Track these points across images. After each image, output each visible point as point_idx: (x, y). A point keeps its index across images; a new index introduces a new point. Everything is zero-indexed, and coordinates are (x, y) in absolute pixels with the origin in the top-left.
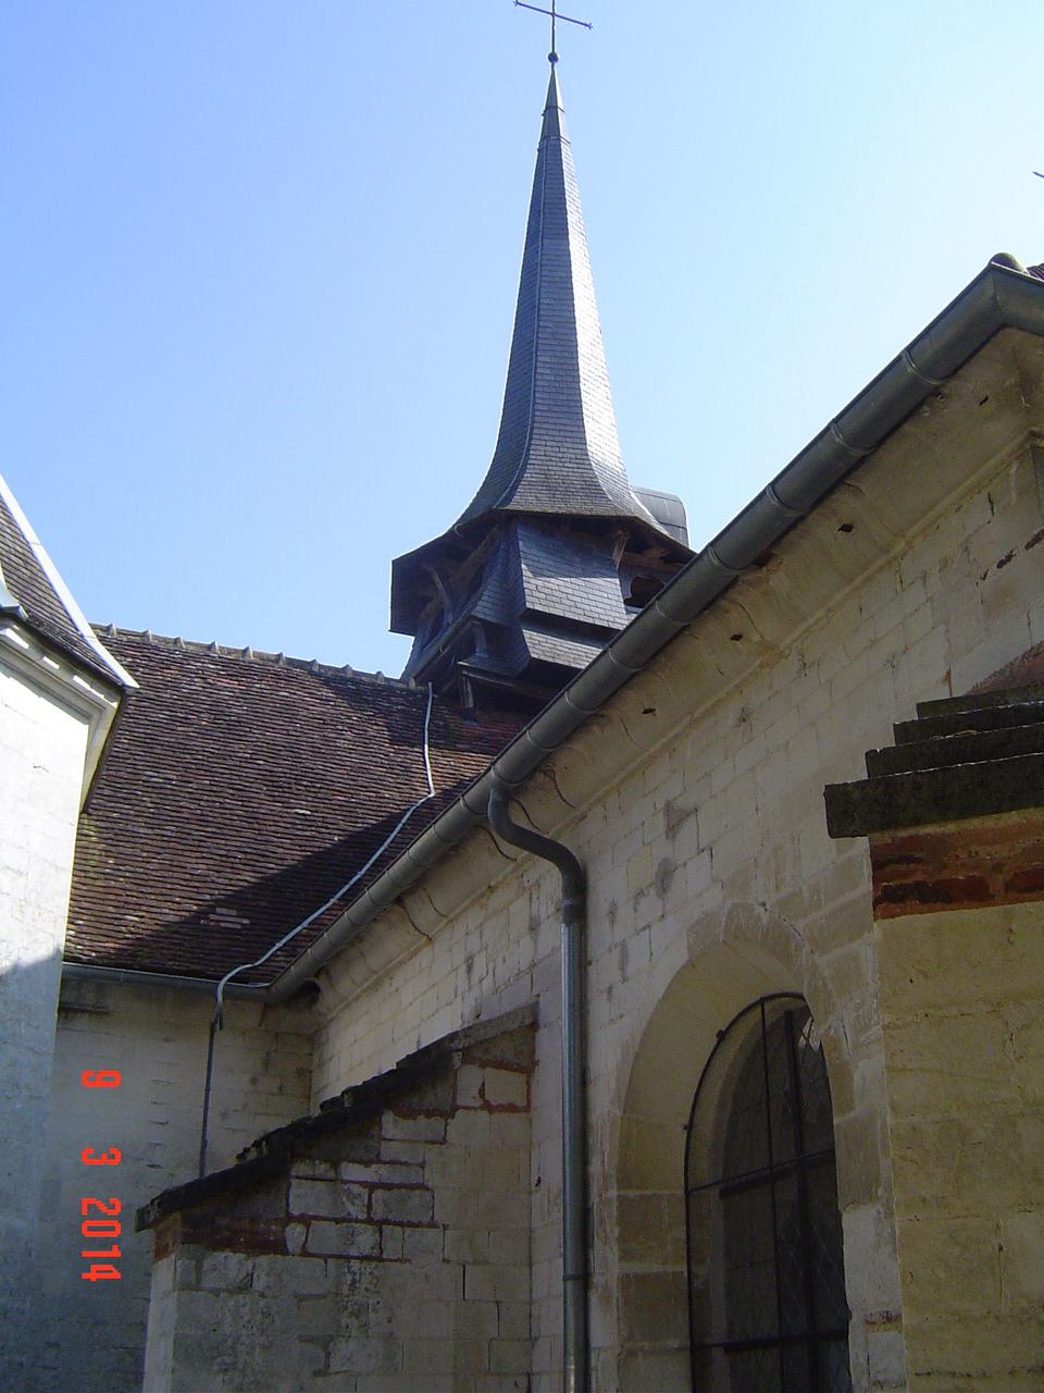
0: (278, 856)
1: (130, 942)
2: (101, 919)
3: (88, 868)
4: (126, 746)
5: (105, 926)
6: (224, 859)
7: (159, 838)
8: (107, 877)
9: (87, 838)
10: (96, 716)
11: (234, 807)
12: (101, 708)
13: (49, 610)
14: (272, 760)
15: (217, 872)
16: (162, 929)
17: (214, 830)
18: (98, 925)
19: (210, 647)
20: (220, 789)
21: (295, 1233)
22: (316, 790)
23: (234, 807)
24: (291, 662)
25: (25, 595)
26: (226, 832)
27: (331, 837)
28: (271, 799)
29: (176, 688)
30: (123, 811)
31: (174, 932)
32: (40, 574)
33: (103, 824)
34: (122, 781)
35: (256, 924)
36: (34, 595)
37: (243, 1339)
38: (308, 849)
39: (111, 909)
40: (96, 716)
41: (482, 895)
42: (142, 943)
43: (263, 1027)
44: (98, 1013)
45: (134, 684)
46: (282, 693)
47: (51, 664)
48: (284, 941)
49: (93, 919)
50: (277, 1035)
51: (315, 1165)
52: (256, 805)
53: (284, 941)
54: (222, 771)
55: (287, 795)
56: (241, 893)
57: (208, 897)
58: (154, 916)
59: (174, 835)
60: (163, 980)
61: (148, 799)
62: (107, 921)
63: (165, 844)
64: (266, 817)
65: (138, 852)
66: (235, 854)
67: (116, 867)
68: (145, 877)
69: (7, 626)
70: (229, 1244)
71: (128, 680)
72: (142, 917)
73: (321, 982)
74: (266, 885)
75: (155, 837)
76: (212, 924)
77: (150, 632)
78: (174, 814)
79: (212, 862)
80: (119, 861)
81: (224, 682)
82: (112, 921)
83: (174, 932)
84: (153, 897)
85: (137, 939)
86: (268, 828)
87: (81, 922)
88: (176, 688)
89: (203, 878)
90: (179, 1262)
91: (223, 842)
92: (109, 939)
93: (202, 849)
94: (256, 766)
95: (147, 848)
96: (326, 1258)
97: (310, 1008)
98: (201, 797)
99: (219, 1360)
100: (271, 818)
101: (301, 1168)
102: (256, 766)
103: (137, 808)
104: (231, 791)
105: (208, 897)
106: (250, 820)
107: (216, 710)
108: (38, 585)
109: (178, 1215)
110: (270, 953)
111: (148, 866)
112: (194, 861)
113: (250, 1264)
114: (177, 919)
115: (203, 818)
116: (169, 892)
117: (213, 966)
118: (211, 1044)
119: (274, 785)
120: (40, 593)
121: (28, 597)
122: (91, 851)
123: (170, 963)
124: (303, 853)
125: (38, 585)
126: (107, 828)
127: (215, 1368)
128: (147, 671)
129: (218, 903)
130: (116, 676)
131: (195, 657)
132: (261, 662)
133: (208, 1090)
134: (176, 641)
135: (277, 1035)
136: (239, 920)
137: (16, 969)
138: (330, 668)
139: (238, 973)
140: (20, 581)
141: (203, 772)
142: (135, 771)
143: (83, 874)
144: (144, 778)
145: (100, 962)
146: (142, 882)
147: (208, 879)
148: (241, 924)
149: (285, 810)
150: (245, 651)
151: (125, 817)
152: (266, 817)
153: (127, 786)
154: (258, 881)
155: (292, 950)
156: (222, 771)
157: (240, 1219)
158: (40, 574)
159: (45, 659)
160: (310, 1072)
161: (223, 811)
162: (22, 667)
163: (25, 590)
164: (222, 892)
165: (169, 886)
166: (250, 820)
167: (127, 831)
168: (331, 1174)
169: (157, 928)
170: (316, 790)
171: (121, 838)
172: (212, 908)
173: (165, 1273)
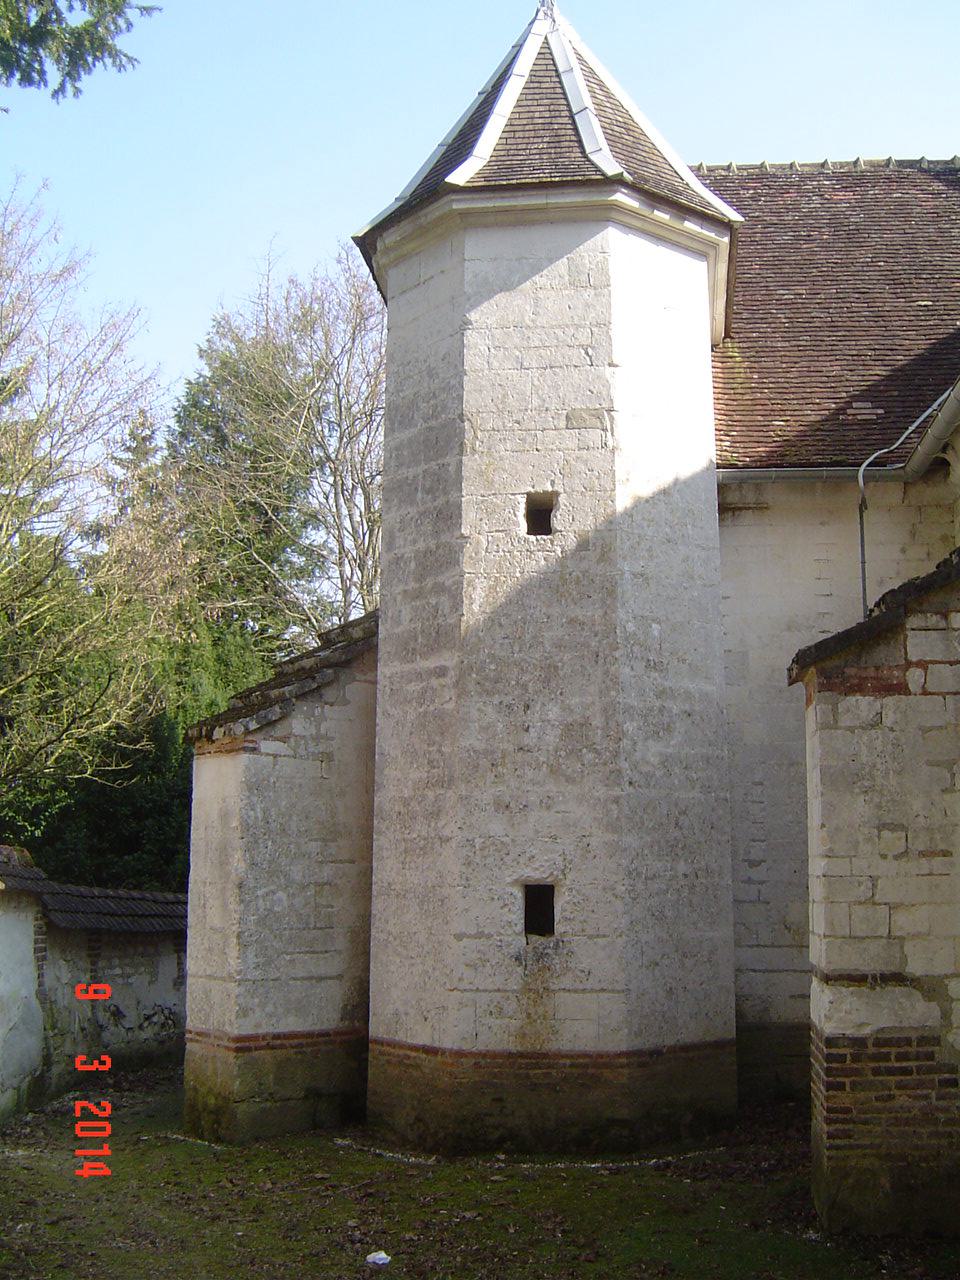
0: (904, 348)
1: (777, 444)
2: (750, 428)
3: (735, 386)
4: (757, 271)
5: (755, 434)
6: (855, 358)
7: (796, 348)
8: (754, 390)
9: (733, 359)
10: (712, 253)
11: (861, 310)
12: (715, 246)
13: (653, 167)
14: (892, 260)
15: (851, 371)
16: (806, 428)
17: (844, 333)
18: (750, 433)
19: (823, 165)
20: (847, 295)
21: (914, 677)
22: (935, 280)
23: (861, 310)
24: (901, 163)
25: (630, 159)
26: (857, 333)
27: (954, 322)
28: (894, 296)
29: (798, 210)
30: (762, 330)
31: (818, 430)
32: (642, 137)
33: (745, 345)
34: (758, 303)
35: (889, 412)
36: (639, 157)
37: (879, 766)
38: (933, 337)
39: (760, 418)
40: (712, 253)
41: (594, 416)
42: (789, 443)
43: (906, 502)
44: (761, 508)
45: (740, 218)
46: (895, 195)
47: (662, 216)
48: (916, 424)
49: (744, 428)
50: (920, 508)
51: (927, 618)
52: (881, 305)
53: (916, 424)
54: (845, 278)
55: (909, 290)
56: (869, 389)
57: (844, 395)
58: (798, 418)
59: (809, 343)
60: (746, 474)
61: (782, 316)
62: (757, 429)
63: (802, 354)
64: (891, 314)
65: (778, 364)
66: (865, 352)
67: (761, 381)
68: (786, 385)
69: (615, 192)
70: (858, 688)
71: (734, 216)
72: (787, 421)
73: (949, 456)
74: (898, 377)
75: (791, 349)
76: (850, 418)
77: (767, 164)
78: (807, 325)
79: (845, 362)
80: (762, 375)
81: (841, 195)
82: (761, 428)
83: (818, 430)
84: (795, 402)
85: (785, 441)
86: (894, 323)
87: (735, 433)
88: (798, 210)
89: (838, 379)
90: (818, 707)
91: (854, 343)
92: (760, 445)
93: (834, 353)
94: (877, 268)
95: (786, 359)
96: (944, 695)
97: (945, 481)
98: (830, 306)
99: (859, 784)
100: (896, 314)
101: (913, 621)
102: (877, 268)
103: (773, 325)
104: (857, 295)
105: (844, 395)
106: (876, 319)
107: (836, 223)
108: (641, 147)
109: (813, 670)
110: (904, 436)
111: (788, 375)
112: (828, 364)
113: (878, 705)
114: (819, 418)
115: (833, 324)
116: (809, 395)
117: (853, 455)
118: (861, 517)
119: (895, 282)
120: (644, 154)
121: (634, 161)
122: (736, 370)
123: (814, 457)
124: (929, 342)
125: (641, 147)
126: (748, 348)
127: (857, 790)
128: (768, 199)
129: (855, 398)
130: (722, 214)
131: (811, 177)
132: (873, 169)
133: (863, 562)
134: (792, 165)
135: (920, 508)
136: (874, 411)
137: (676, 482)
138: (938, 162)
139: (875, 458)
140: (624, 148)
141: (829, 282)
142: (768, 292)
143: (732, 391)
144: (777, 297)
145: (754, 465)
146: (784, 390)
147: (843, 378)
148: (877, 414)
149: (908, 304)
150: (856, 163)
151: (763, 335)
152: (891, 314)
153: (763, 307)
154: (888, 373)
155: (921, 431)
156: (845, 278)
157: (866, 668)
158: (642, 137)
159: (656, 212)
160: (954, 537)
161: (850, 315)
162: (638, 224)
163: (630, 155)
164: (857, 388)
165: (808, 390)
166: (876, 319)
167: (767, 347)
168: (942, 624)
169: (802, 428)
170: (935, 280)
171: (762, 354)
172: (849, 405)
173: (812, 717)
